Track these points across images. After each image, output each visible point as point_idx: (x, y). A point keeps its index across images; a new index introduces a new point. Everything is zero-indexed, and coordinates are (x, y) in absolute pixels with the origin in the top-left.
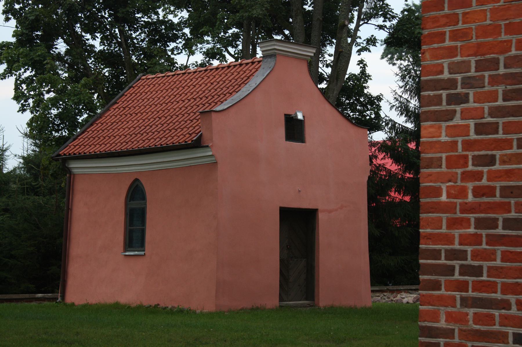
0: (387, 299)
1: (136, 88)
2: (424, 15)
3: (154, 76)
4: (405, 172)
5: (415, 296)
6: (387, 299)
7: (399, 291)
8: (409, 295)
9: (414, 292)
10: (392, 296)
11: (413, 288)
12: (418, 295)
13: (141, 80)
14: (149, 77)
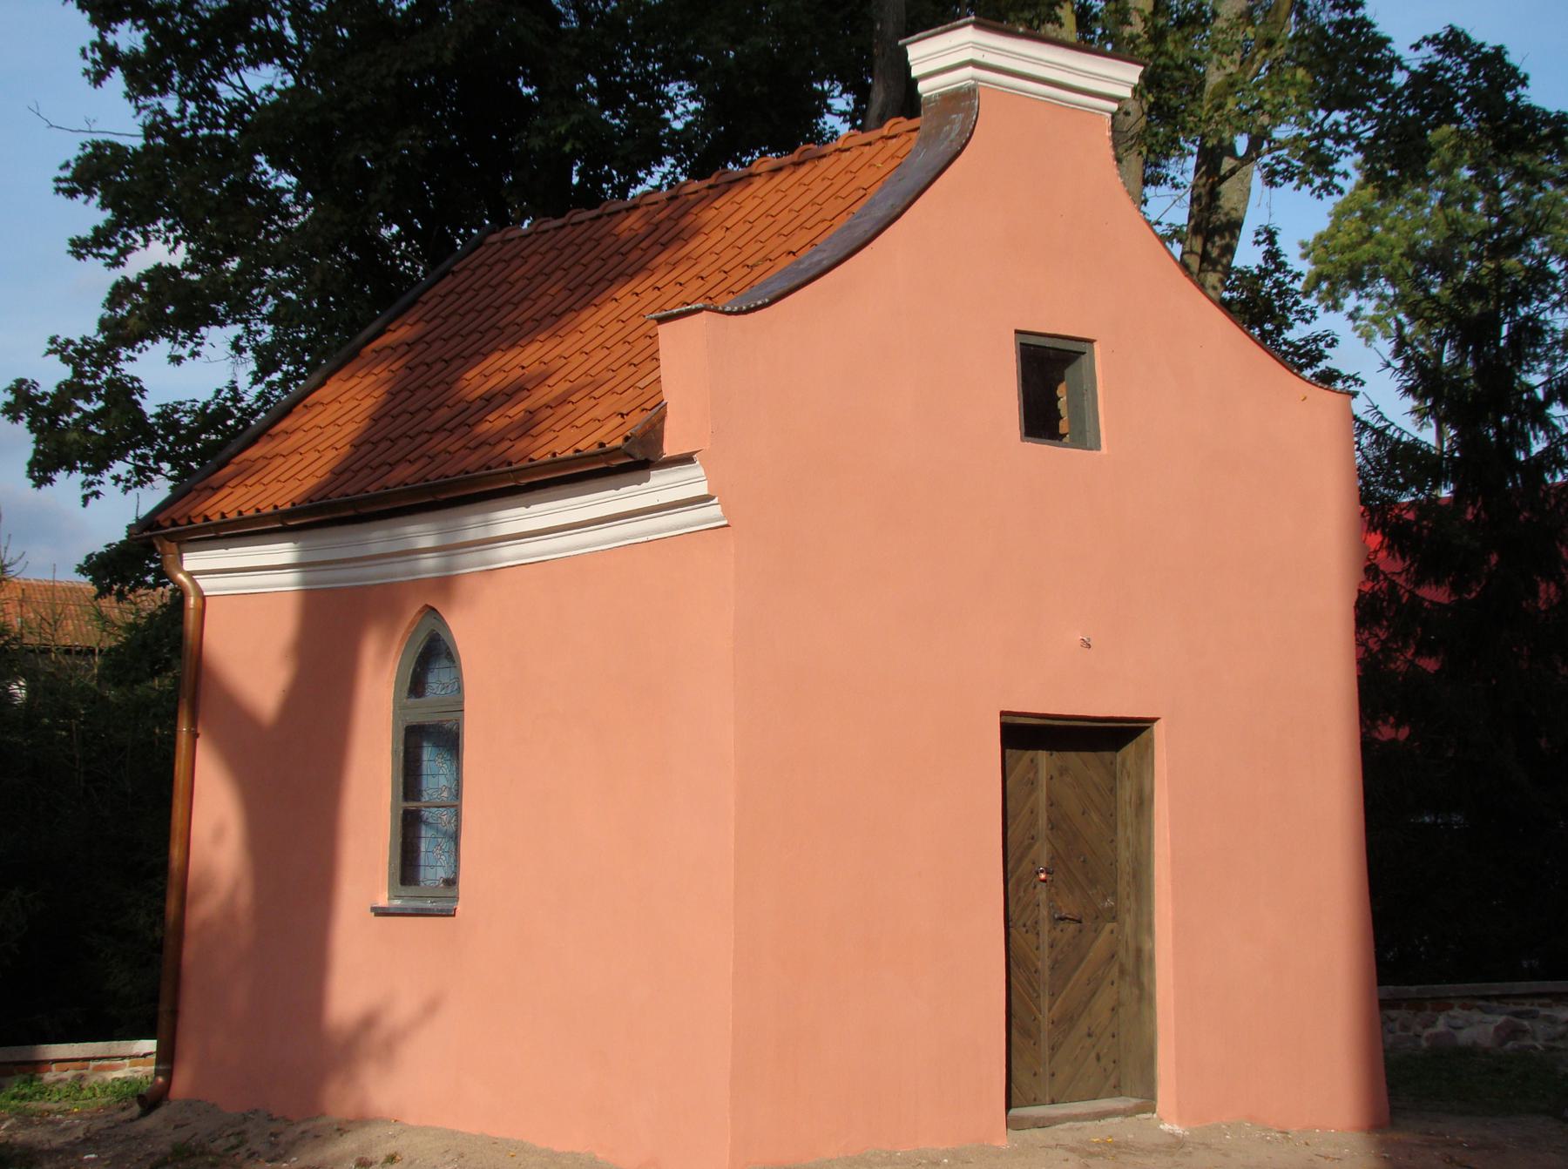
0: (1399, 1033)
1: (461, 277)
2: (1058, 1003)
3: (559, 222)
5: (1501, 1019)
6: (1399, 1033)
7: (1442, 1004)
8: (1476, 1016)
9: (1495, 1004)
10: (1418, 1020)
12: (1511, 1018)
13: (483, 249)
14: (576, 219)
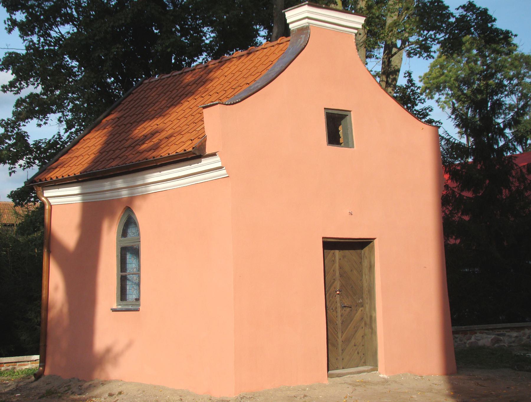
0: (459, 342)
4: (462, 191)
5: (493, 337)
6: (459, 342)
7: (473, 332)
8: (485, 336)
11: (490, 328)
12: (496, 336)
